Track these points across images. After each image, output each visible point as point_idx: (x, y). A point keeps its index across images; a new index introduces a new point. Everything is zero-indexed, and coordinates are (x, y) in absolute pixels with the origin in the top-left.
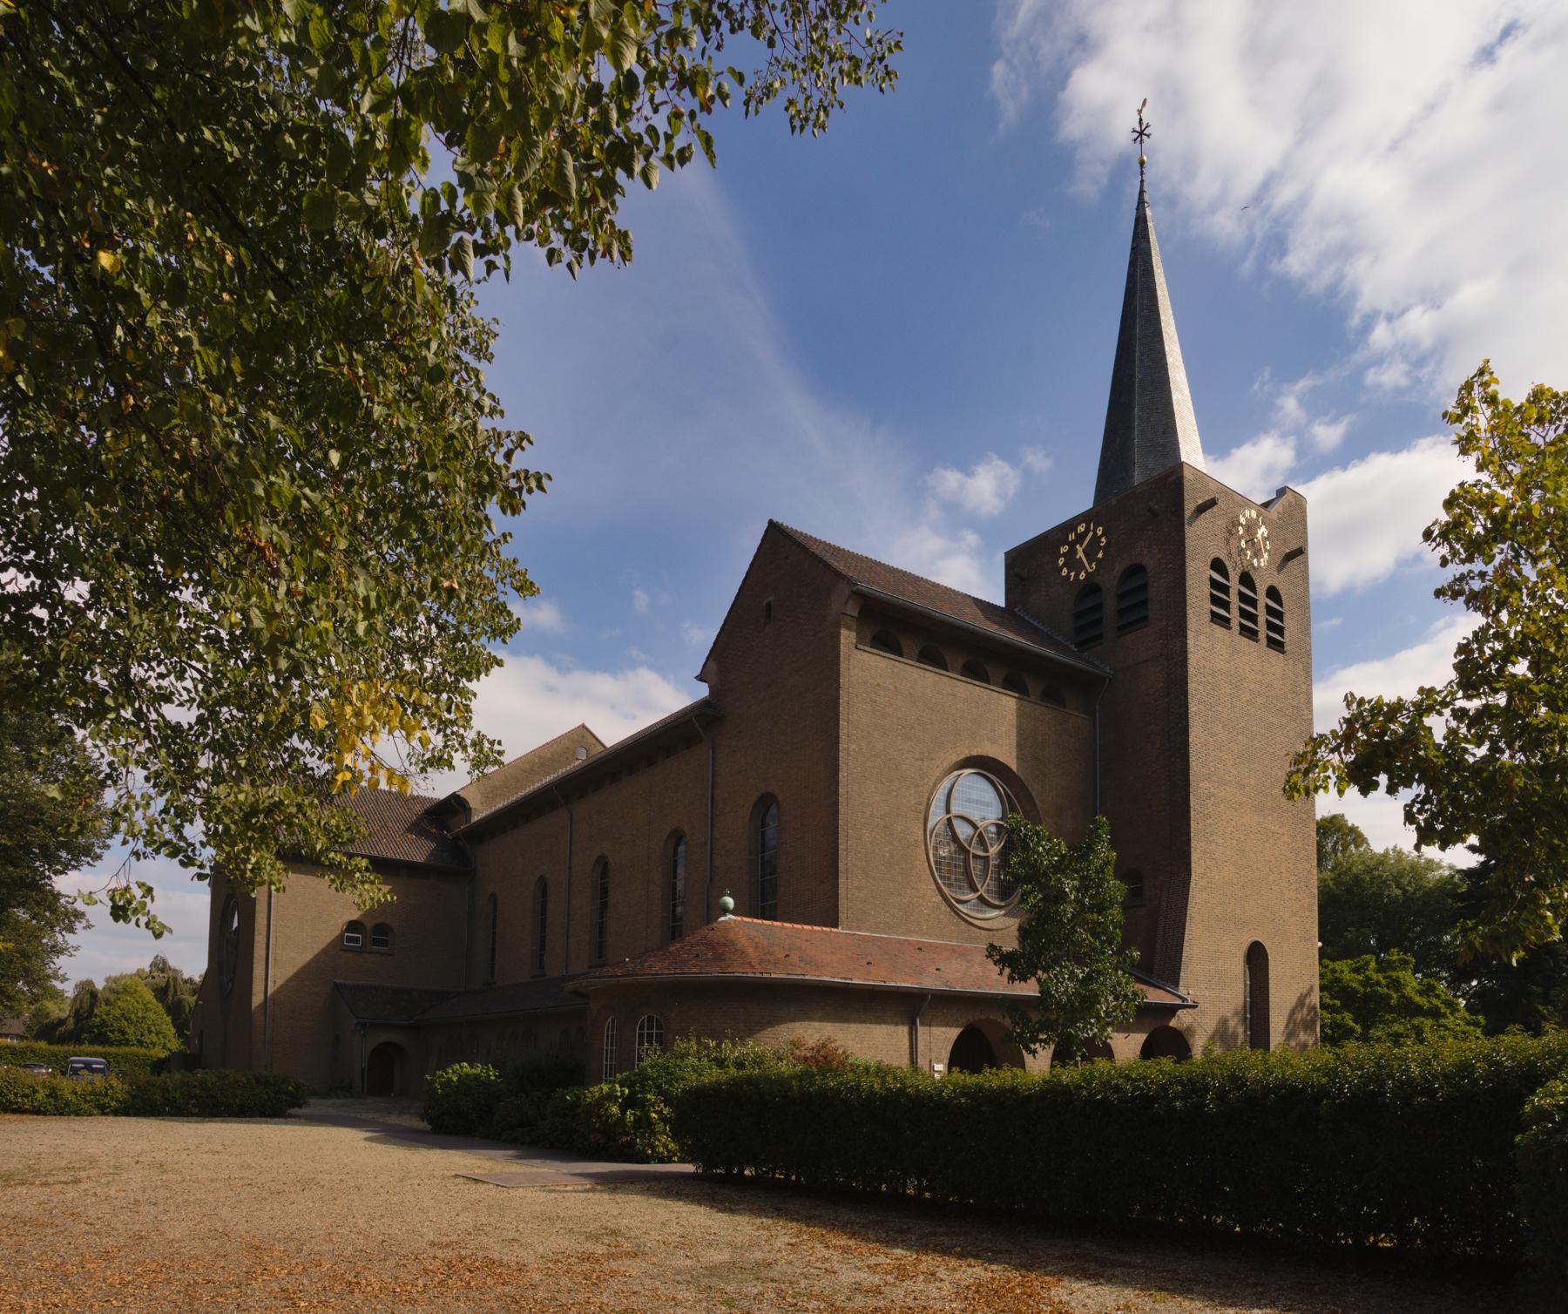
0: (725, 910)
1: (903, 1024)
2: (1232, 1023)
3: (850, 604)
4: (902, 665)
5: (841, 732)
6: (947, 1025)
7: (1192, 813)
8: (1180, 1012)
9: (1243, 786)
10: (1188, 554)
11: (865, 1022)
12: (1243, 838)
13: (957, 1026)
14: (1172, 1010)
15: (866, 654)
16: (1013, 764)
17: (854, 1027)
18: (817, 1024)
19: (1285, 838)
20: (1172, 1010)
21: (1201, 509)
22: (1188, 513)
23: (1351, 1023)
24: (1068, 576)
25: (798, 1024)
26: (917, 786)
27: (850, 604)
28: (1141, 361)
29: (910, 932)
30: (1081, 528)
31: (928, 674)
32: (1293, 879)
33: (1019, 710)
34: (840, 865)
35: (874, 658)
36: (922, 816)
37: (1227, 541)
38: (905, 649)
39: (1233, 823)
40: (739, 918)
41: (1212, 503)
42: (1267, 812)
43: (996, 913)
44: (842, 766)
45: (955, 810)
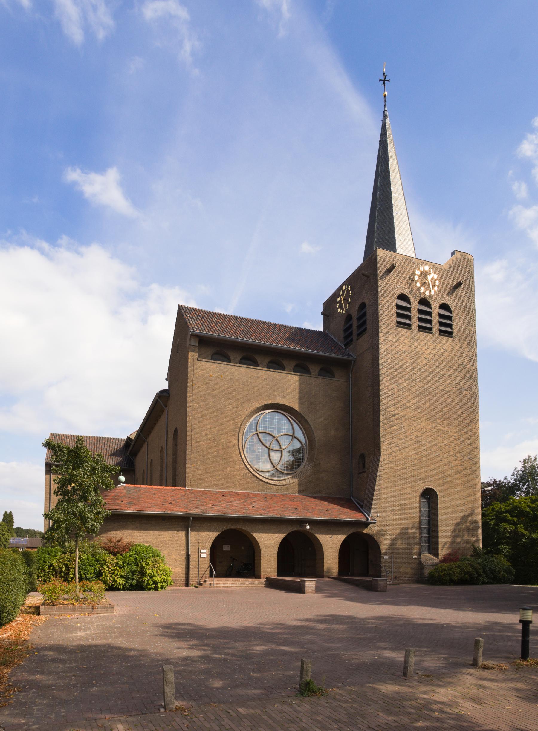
0: (120, 482)
1: (182, 531)
2: (410, 531)
3: (192, 340)
4: (226, 366)
5: (188, 399)
6: (343, 535)
7: (381, 424)
8: (371, 525)
9: (420, 408)
10: (380, 294)
11: (159, 530)
12: (419, 435)
13: (346, 535)
14: (366, 525)
15: (203, 363)
16: (296, 407)
17: (151, 532)
18: (130, 532)
19: (453, 434)
20: (366, 525)
21: (390, 270)
22: (380, 274)
23: (523, 531)
24: (340, 312)
25: (119, 531)
26: (234, 420)
27: (192, 340)
28: (380, 198)
29: (228, 487)
30: (344, 288)
31: (241, 368)
32: (458, 455)
33: (300, 380)
34: (187, 458)
35: (208, 364)
36: (237, 434)
37: (410, 284)
38: (232, 358)
39: (412, 428)
40: (128, 485)
41: (393, 267)
42: (438, 421)
43: (289, 477)
44: (188, 413)
45: (259, 430)
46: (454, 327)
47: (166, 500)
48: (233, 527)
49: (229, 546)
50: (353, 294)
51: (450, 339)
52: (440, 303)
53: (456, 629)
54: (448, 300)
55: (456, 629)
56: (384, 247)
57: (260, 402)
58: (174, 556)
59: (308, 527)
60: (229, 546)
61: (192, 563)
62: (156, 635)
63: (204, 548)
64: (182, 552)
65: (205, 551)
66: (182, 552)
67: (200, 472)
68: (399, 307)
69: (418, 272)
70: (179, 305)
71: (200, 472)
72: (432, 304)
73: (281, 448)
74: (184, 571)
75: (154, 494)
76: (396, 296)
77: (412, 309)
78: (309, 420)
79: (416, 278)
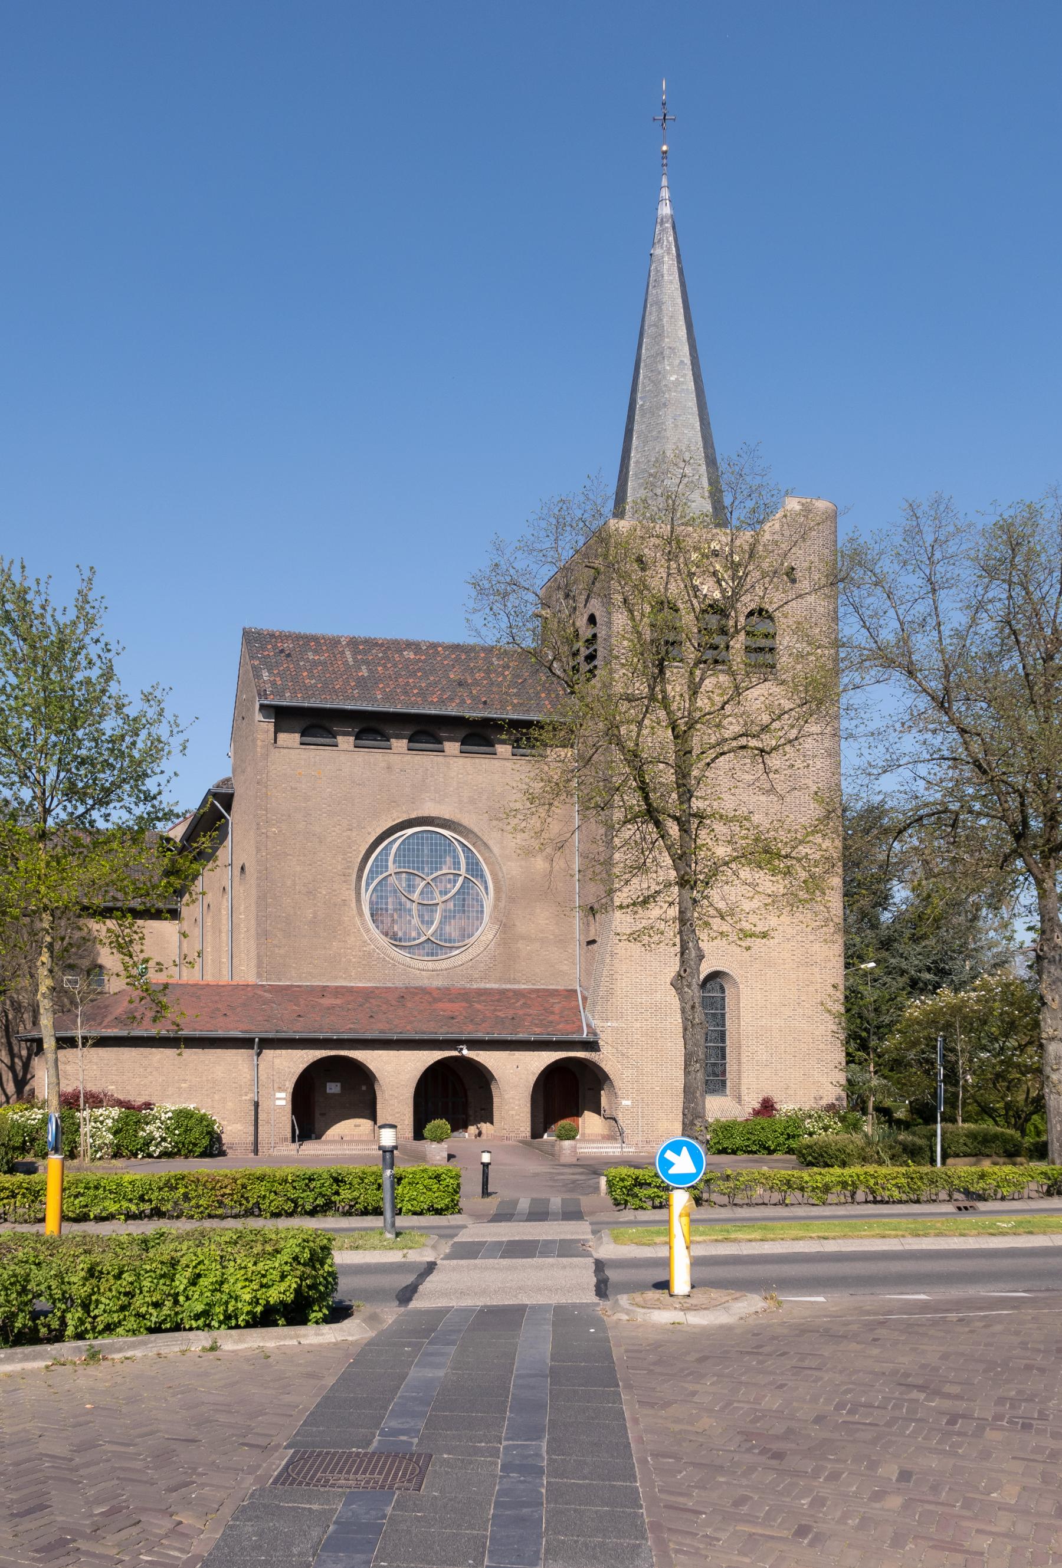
47: (218, 1009)
49: (339, 1084)
57: (395, 815)
58: (230, 1104)
60: (339, 1084)
62: (829, 1011)
63: (280, 1090)
65: (283, 1095)
67: (282, 952)
70: (244, 629)
71: (282, 952)
75: (198, 997)
78: (491, 843)
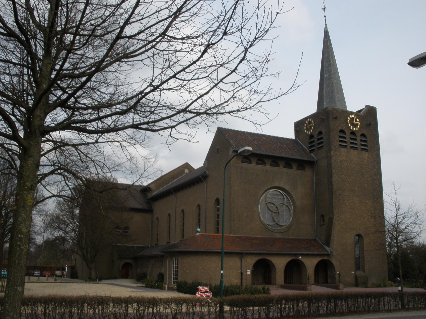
19: (370, 204)
46: (369, 146)
48: (263, 258)
50: (315, 125)
51: (367, 153)
52: (361, 134)
53: (401, 272)
54: (364, 132)
55: (401, 272)
56: (383, 219)
59: (300, 257)
61: (244, 277)
63: (249, 269)
64: (238, 271)
66: (238, 271)
68: (340, 137)
69: (349, 119)
72: (357, 134)
73: (278, 211)
74: (240, 281)
76: (339, 131)
77: (347, 138)
79: (348, 121)
